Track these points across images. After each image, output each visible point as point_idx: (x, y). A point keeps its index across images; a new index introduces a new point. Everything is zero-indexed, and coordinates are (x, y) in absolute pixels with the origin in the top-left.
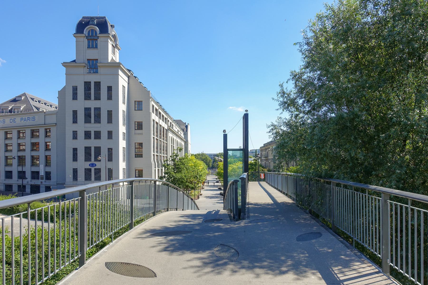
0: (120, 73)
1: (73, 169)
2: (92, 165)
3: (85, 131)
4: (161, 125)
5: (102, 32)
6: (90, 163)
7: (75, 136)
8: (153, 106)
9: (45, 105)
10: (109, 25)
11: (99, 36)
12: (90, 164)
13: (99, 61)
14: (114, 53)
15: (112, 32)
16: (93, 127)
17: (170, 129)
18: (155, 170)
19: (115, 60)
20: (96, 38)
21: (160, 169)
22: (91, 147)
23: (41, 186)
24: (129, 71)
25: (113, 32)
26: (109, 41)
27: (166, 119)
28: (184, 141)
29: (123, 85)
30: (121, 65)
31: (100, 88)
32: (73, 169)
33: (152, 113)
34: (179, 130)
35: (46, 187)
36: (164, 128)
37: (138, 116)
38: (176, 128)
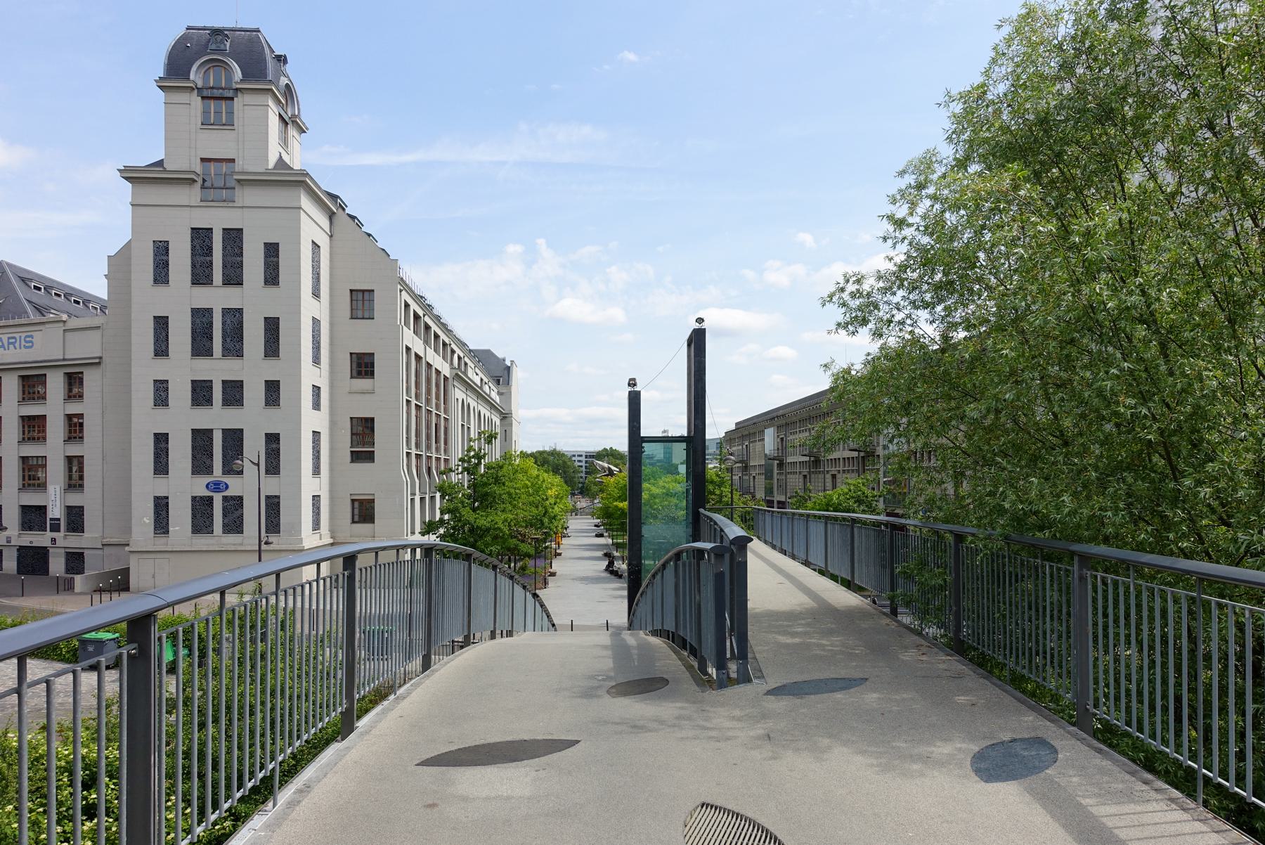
2: (217, 487)
6: (208, 479)
7: (161, 393)
8: (407, 305)
16: (217, 369)
22: (211, 431)
23: (51, 550)
24: (334, 197)
27: (445, 344)
29: (313, 242)
34: (485, 380)
35: (68, 554)
36: (438, 372)
38: (475, 375)
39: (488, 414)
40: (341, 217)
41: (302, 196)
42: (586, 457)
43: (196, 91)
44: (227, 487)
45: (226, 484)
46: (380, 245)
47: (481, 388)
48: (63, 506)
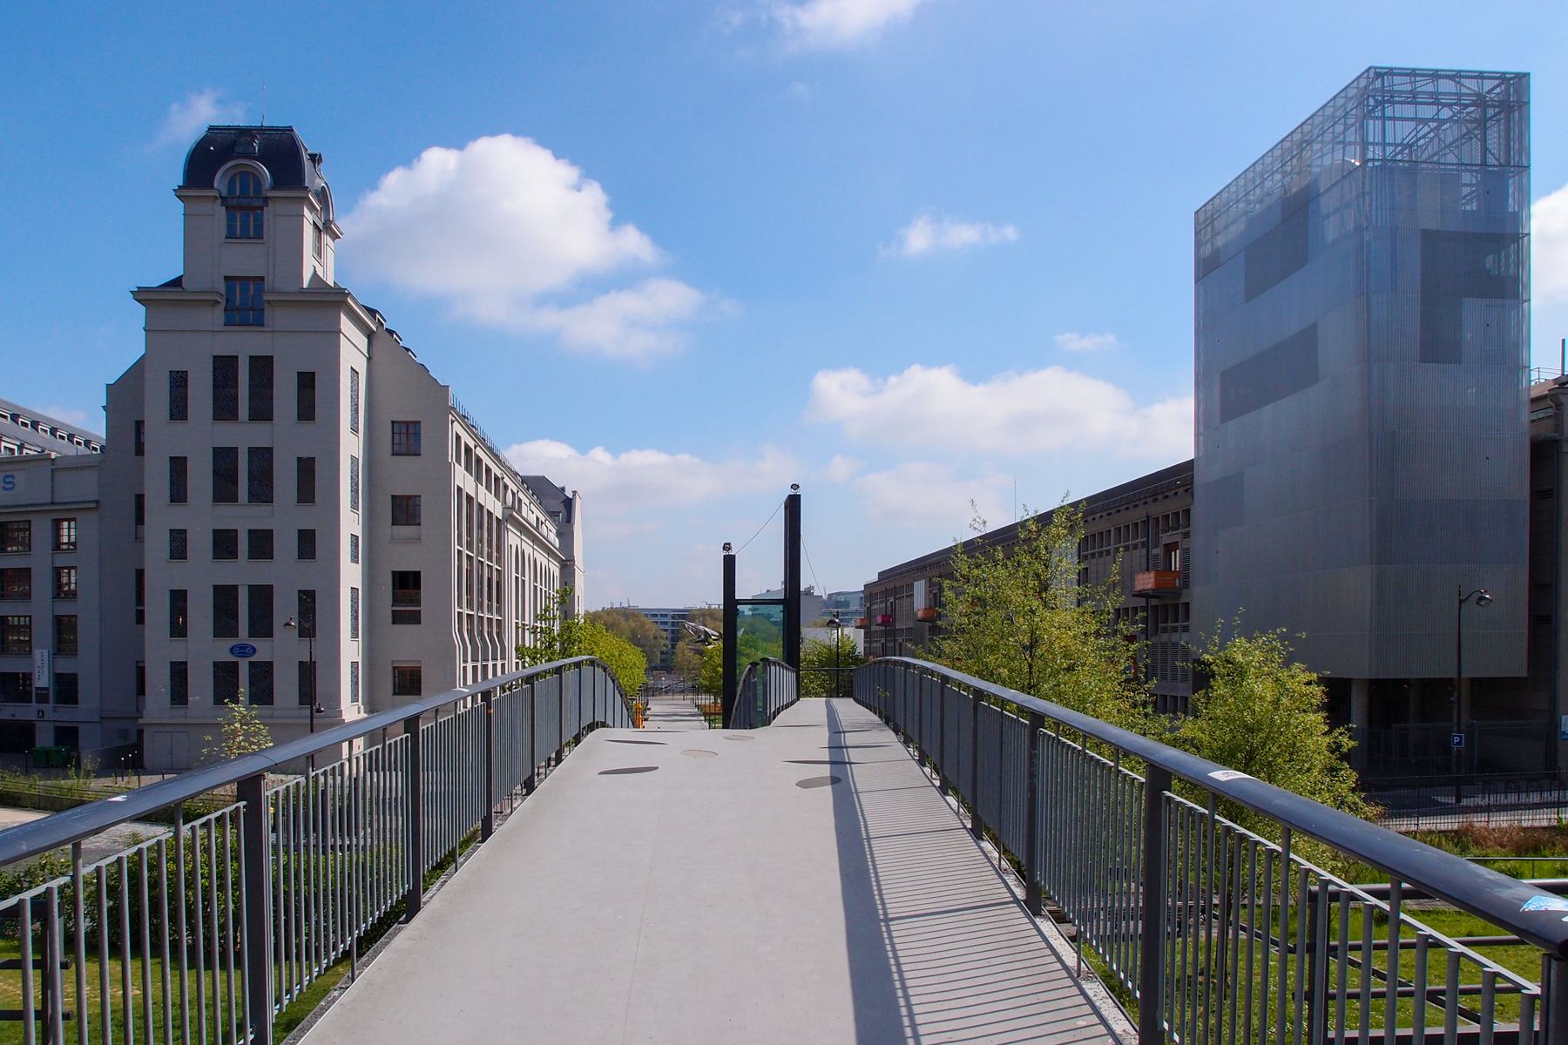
0: (346, 324)
1: (171, 663)
2: (243, 651)
3: (215, 532)
4: (492, 511)
5: (278, 183)
6: (231, 642)
7: (179, 545)
8: (458, 437)
9: (14, 421)
10: (305, 157)
11: (271, 198)
12: (232, 648)
13: (267, 285)
14: (319, 252)
15: (315, 179)
16: (242, 517)
17: (511, 517)
18: (465, 668)
19: (322, 276)
20: (257, 203)
21: (479, 665)
22: (235, 587)
23: (38, 725)
24: (372, 312)
25: (318, 180)
26: (306, 212)
27: (497, 479)
28: (561, 561)
29: (352, 368)
30: (349, 300)
31: (271, 379)
32: (171, 663)
33: (456, 464)
34: (542, 518)
35: (57, 729)
36: (490, 514)
37: (404, 476)
38: (531, 513)
39: (545, 562)
40: (382, 340)
41: (342, 315)
42: (673, 626)
43: (220, 200)
44: (231, 650)
45: (253, 648)
46: (418, 360)
47: (537, 529)
48: (51, 674)
